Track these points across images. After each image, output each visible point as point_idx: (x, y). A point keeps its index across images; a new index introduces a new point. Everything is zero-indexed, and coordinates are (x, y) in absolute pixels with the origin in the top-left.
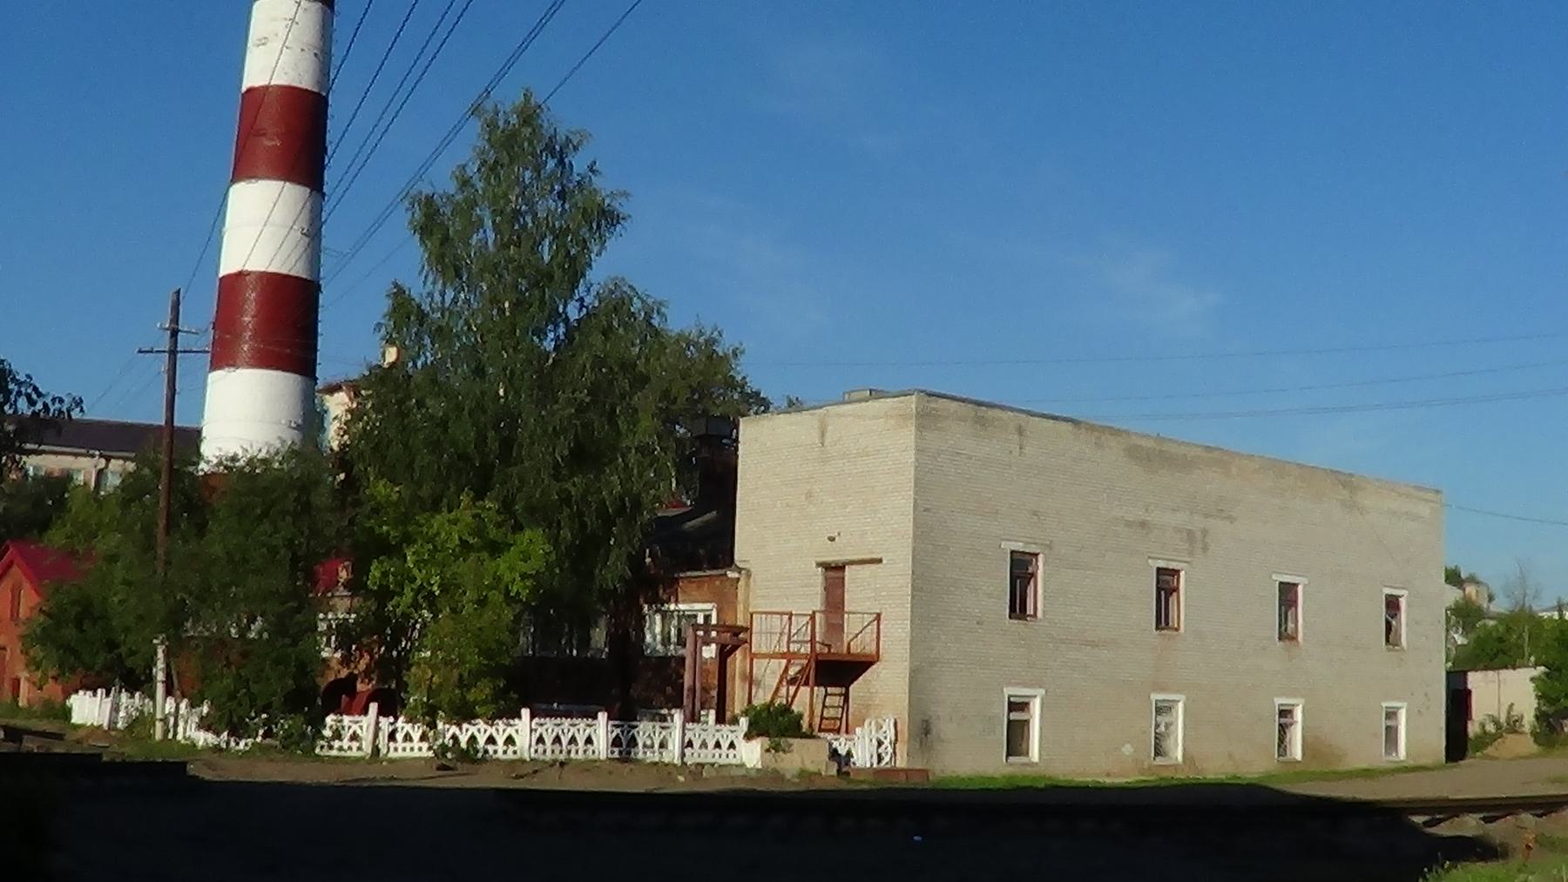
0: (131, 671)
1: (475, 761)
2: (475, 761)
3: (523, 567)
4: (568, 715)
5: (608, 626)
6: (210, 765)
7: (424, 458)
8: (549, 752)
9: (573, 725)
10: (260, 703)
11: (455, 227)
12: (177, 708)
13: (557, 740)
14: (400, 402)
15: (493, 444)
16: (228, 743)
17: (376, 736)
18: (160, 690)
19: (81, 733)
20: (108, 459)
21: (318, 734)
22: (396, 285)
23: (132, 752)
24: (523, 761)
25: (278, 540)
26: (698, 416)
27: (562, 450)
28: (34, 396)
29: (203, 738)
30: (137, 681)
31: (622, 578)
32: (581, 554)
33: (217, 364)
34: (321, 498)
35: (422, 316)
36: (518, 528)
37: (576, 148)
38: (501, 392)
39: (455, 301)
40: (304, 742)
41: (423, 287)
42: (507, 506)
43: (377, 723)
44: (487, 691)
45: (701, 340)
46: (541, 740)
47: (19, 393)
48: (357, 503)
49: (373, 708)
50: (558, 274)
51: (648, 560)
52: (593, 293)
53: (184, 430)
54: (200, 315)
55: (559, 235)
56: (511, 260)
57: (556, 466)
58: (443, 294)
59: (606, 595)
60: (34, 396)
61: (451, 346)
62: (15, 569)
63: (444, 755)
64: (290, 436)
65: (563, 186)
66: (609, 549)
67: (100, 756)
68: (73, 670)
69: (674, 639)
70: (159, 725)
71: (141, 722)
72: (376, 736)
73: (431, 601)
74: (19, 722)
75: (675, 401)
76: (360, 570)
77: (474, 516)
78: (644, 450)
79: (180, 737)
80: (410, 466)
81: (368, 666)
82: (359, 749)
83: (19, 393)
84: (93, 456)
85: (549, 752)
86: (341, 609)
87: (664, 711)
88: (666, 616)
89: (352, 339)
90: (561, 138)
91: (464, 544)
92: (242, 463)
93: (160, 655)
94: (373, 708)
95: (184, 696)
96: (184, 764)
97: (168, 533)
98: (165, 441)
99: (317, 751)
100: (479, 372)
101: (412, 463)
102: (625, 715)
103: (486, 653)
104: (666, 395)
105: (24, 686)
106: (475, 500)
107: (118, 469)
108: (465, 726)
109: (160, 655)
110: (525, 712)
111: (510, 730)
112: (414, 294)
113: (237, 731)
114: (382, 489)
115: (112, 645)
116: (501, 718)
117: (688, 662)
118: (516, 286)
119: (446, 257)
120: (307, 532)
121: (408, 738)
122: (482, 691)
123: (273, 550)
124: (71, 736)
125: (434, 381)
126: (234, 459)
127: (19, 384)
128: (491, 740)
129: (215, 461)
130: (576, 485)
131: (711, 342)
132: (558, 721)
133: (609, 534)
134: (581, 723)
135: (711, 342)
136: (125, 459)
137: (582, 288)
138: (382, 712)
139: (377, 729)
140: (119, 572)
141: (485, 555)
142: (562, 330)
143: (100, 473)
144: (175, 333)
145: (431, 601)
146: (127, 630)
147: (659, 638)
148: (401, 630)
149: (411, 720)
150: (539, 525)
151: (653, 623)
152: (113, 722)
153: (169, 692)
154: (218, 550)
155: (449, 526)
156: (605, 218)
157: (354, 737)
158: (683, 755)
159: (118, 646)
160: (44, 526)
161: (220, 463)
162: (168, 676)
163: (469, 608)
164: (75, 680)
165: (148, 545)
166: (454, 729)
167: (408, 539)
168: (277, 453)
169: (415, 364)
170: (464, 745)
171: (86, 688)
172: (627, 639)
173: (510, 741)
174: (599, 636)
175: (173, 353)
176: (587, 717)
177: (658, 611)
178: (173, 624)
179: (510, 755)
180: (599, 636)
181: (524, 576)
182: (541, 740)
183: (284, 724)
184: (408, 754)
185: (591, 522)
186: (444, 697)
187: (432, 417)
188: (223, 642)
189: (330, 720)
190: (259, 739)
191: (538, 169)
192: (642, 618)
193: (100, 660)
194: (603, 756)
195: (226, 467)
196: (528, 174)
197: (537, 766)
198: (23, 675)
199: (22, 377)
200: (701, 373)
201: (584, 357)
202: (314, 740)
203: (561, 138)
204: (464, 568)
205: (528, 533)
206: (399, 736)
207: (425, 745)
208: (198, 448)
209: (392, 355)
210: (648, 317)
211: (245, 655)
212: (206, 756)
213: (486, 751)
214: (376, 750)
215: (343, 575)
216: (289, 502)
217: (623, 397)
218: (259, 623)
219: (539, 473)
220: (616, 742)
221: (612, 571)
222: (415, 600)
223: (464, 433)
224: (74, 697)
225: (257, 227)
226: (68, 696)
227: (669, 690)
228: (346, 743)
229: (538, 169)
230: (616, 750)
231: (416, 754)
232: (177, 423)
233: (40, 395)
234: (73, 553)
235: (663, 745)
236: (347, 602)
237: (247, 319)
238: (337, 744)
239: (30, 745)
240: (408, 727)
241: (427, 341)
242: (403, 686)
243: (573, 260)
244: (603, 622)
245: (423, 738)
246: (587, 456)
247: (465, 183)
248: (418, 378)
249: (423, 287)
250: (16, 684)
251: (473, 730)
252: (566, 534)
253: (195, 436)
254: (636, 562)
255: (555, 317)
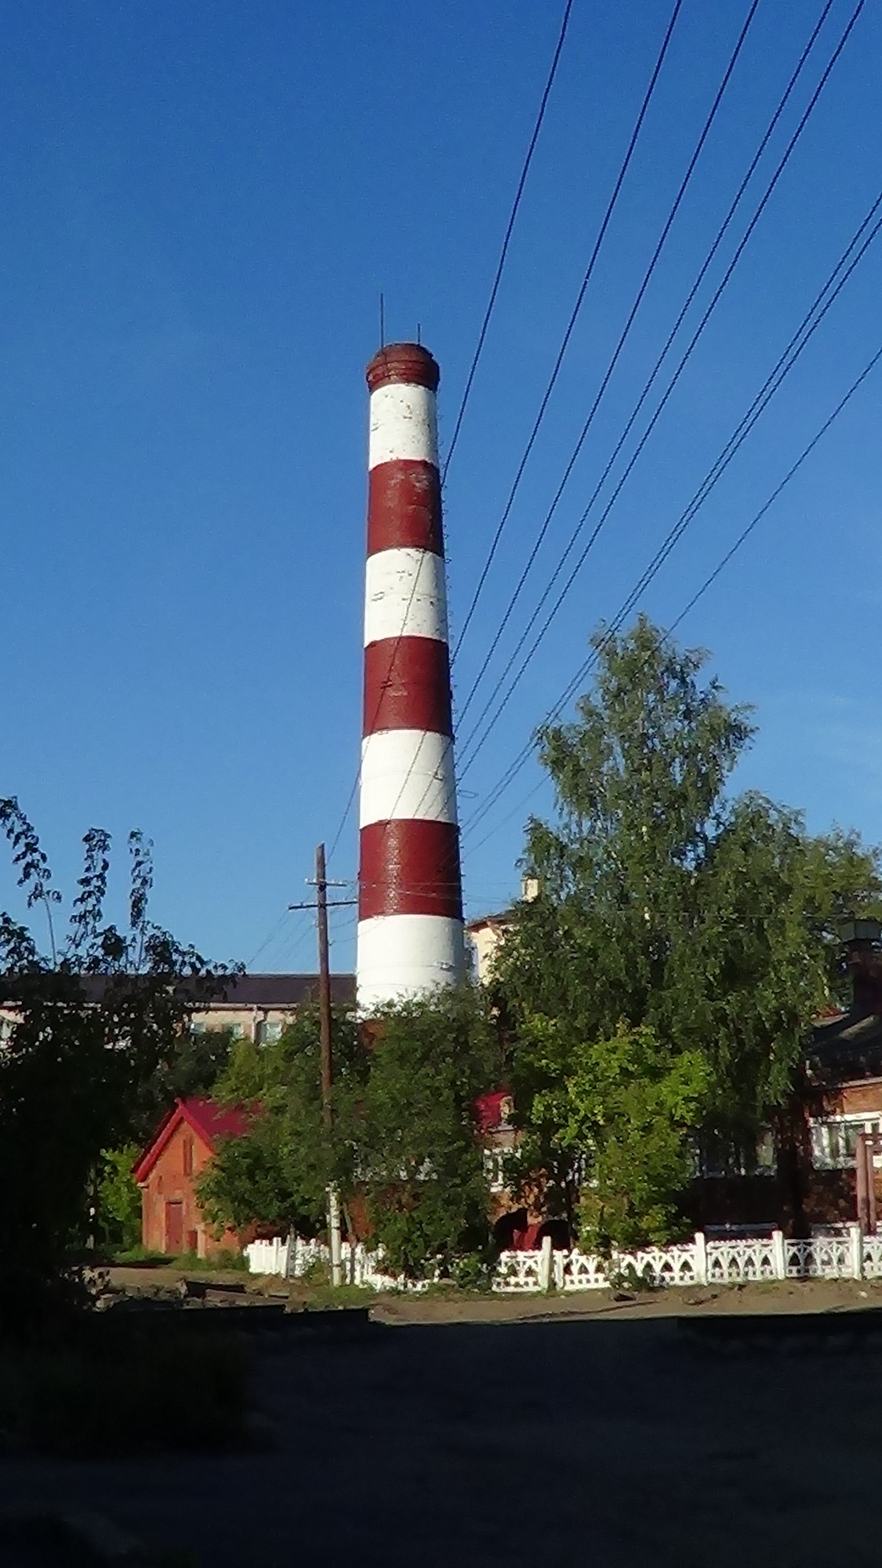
0: (306, 1218)
1: (652, 1289)
2: (652, 1289)
3: (686, 1090)
4: (741, 1236)
5: (775, 1142)
6: (390, 1310)
7: (577, 989)
8: (726, 1275)
9: (749, 1247)
10: (436, 1244)
11: (585, 756)
12: (353, 1253)
13: (734, 1262)
14: (549, 935)
15: (646, 971)
16: (405, 1286)
17: (551, 1270)
18: (335, 1235)
19: (260, 1283)
20: (266, 1011)
21: (493, 1272)
22: (532, 820)
23: (314, 1301)
24: (700, 1286)
25: (439, 1081)
26: (845, 921)
27: (714, 968)
28: (198, 965)
29: (381, 1282)
30: (312, 1228)
31: (784, 1094)
32: (743, 1072)
33: (365, 914)
34: (479, 1037)
35: (562, 849)
36: (676, 1051)
37: (696, 666)
38: (647, 916)
39: (592, 830)
40: (479, 1281)
41: (560, 819)
42: (663, 1031)
43: (552, 1256)
44: (660, 1217)
45: (840, 844)
46: (717, 1264)
47: (184, 963)
48: (515, 1039)
49: (547, 1241)
50: (692, 793)
51: (809, 1072)
52: (729, 808)
53: (337, 978)
54: (345, 869)
55: (688, 754)
56: (645, 785)
57: (709, 986)
58: (579, 825)
59: (771, 1111)
60: (198, 965)
61: (593, 876)
62: (185, 1125)
63: (620, 1284)
64: (444, 978)
65: (687, 705)
66: (769, 1064)
67: (282, 1307)
68: (248, 1220)
69: (843, 1151)
70: (336, 1271)
71: (318, 1268)
72: (551, 1270)
73: (596, 1130)
74: (200, 1276)
75: (819, 909)
76: (522, 1104)
77: (631, 1043)
78: (794, 961)
79: (357, 1281)
80: (563, 999)
81: (537, 1198)
82: (536, 1284)
83: (184, 963)
84: (251, 1009)
85: (726, 1275)
86: (507, 1144)
87: (840, 1225)
88: (832, 1127)
89: (495, 877)
90: (680, 659)
91: (624, 1071)
92: (399, 1008)
93: (333, 1201)
94: (547, 1241)
95: (358, 1241)
96: (365, 1311)
97: (332, 1082)
98: (323, 992)
99: (494, 1288)
100: (623, 898)
101: (564, 994)
102: (799, 1232)
103: (654, 1179)
104: (810, 900)
105: (201, 1239)
106: (630, 1027)
107: (277, 1023)
108: (640, 1254)
109: (333, 1201)
110: (699, 1237)
111: (686, 1256)
112: (553, 829)
113: (413, 1273)
114: (538, 1024)
115: (285, 1195)
116: (675, 1244)
117: (860, 1174)
118: (650, 810)
119: (582, 793)
120: (468, 1072)
121: (583, 1270)
122: (655, 1217)
123: (437, 1092)
124: (251, 1287)
125: (581, 913)
126: (390, 1005)
127: (184, 954)
128: (667, 1267)
129: (372, 1008)
130: (730, 1004)
131: (850, 844)
132: (733, 1243)
133: (769, 1050)
134: (757, 1244)
135: (850, 844)
136: (283, 1010)
137: (717, 806)
138: (556, 1246)
139: (552, 1262)
140: (286, 1121)
141: (646, 1080)
142: (701, 849)
143: (259, 1026)
144: (322, 887)
145: (596, 1130)
146: (298, 1179)
147: (827, 1150)
148: (567, 1159)
149: (585, 1252)
150: (698, 1047)
151: (820, 1136)
152: (290, 1269)
153: (344, 1238)
154: (382, 1096)
155: (609, 1054)
156: (736, 732)
157: (530, 1272)
158: (863, 1269)
159: (291, 1195)
160: (209, 1080)
161: (377, 1010)
162: (343, 1221)
163: (636, 1135)
164: (250, 1230)
165: (314, 1095)
166: (629, 1259)
167: (568, 1071)
168: (432, 996)
169: (559, 897)
170: (640, 1274)
171: (262, 1237)
172: (795, 1156)
173: (686, 1266)
174: (766, 1153)
175: (323, 906)
176: (762, 1237)
177: (824, 1123)
178: (343, 1170)
179: (688, 1282)
180: (766, 1153)
181: (687, 1100)
182: (717, 1264)
183: (460, 1263)
184: (585, 1286)
185: (751, 1040)
186: (618, 1226)
187: (581, 947)
188: (395, 1185)
189: (504, 1256)
190: (436, 1280)
191: (660, 691)
192: (808, 1131)
193: (276, 1207)
194: (781, 1276)
195: (384, 1014)
196: (651, 697)
197: (715, 1291)
198: (200, 1227)
199: (184, 948)
200: (842, 877)
201: (726, 876)
202: (490, 1276)
203: (680, 659)
204: (623, 1096)
205: (687, 1056)
206: (575, 1268)
207: (601, 1276)
208: (355, 996)
209: (533, 890)
210: (786, 827)
211: (416, 1197)
212: (385, 1300)
213: (663, 1279)
214: (552, 1284)
215: (506, 1111)
216: (459, 1052)
217: (769, 910)
218: (427, 1165)
219: (692, 995)
220: (794, 1261)
221: (775, 1086)
222: (580, 1131)
223: (613, 960)
224: (250, 1246)
225: (394, 776)
226: (244, 1246)
227: (842, 1203)
228: (521, 1279)
229: (660, 691)
230: (794, 1269)
231: (593, 1285)
232: (330, 972)
233: (202, 963)
234: (241, 1108)
235: (841, 1261)
236: (512, 1135)
237: (728, 1226)
238: (512, 1280)
239: (215, 1300)
240: (583, 1259)
241: (568, 873)
242: (574, 1218)
243: (705, 777)
244: (769, 1138)
245: (599, 1269)
246: (738, 973)
247: (590, 713)
248: (563, 909)
249: (560, 819)
250: (193, 1235)
251: (648, 1258)
252: (725, 1053)
253: (348, 984)
254: (797, 1075)
255: (694, 837)
